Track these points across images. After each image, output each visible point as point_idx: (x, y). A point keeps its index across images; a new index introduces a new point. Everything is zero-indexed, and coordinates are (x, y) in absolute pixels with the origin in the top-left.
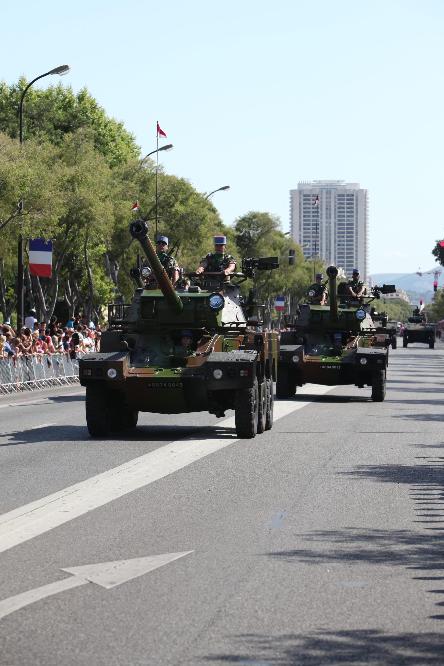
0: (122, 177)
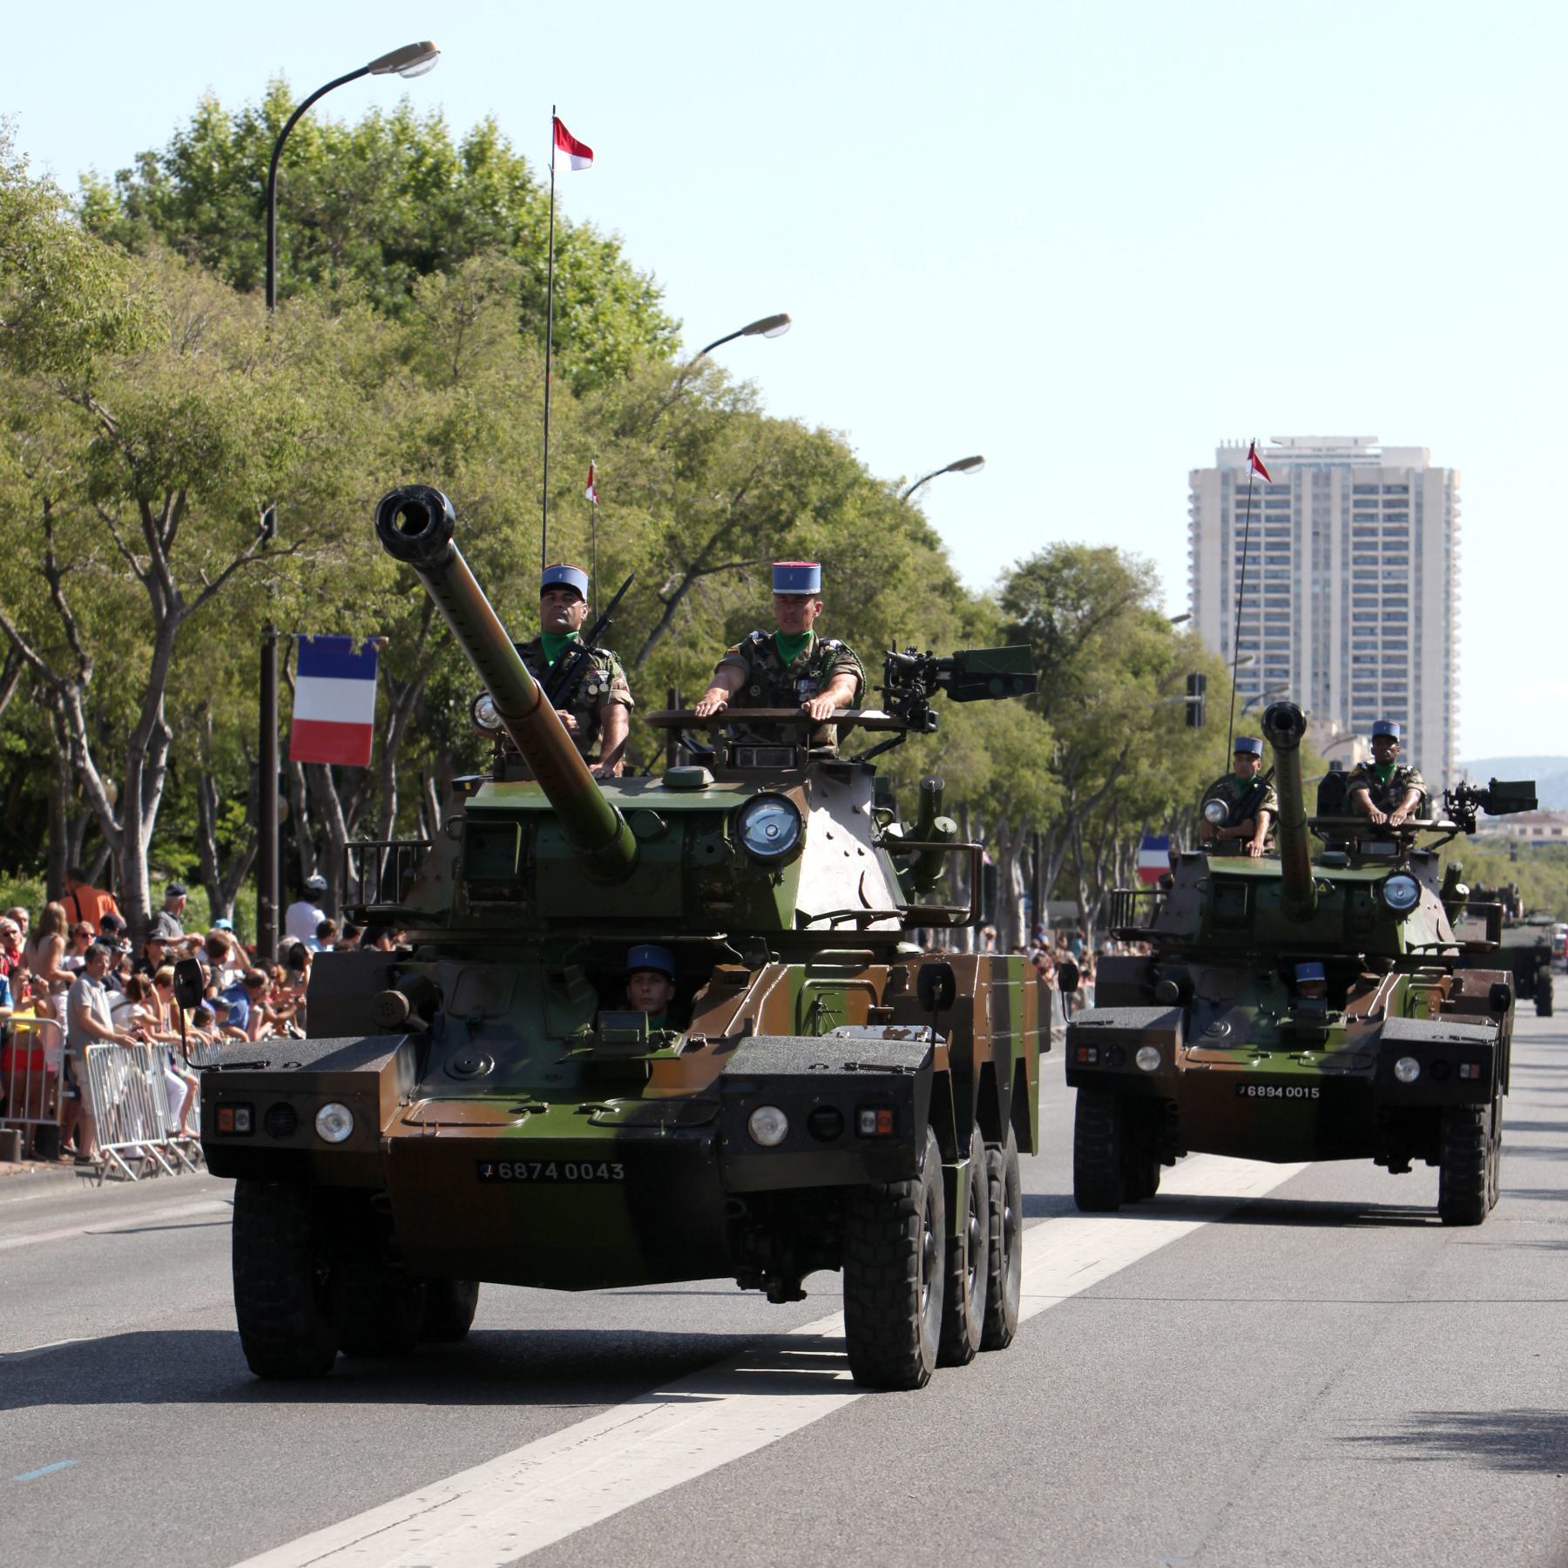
0: (615, 425)
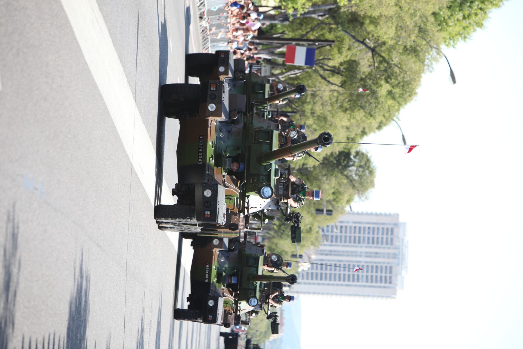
0: (422, 26)
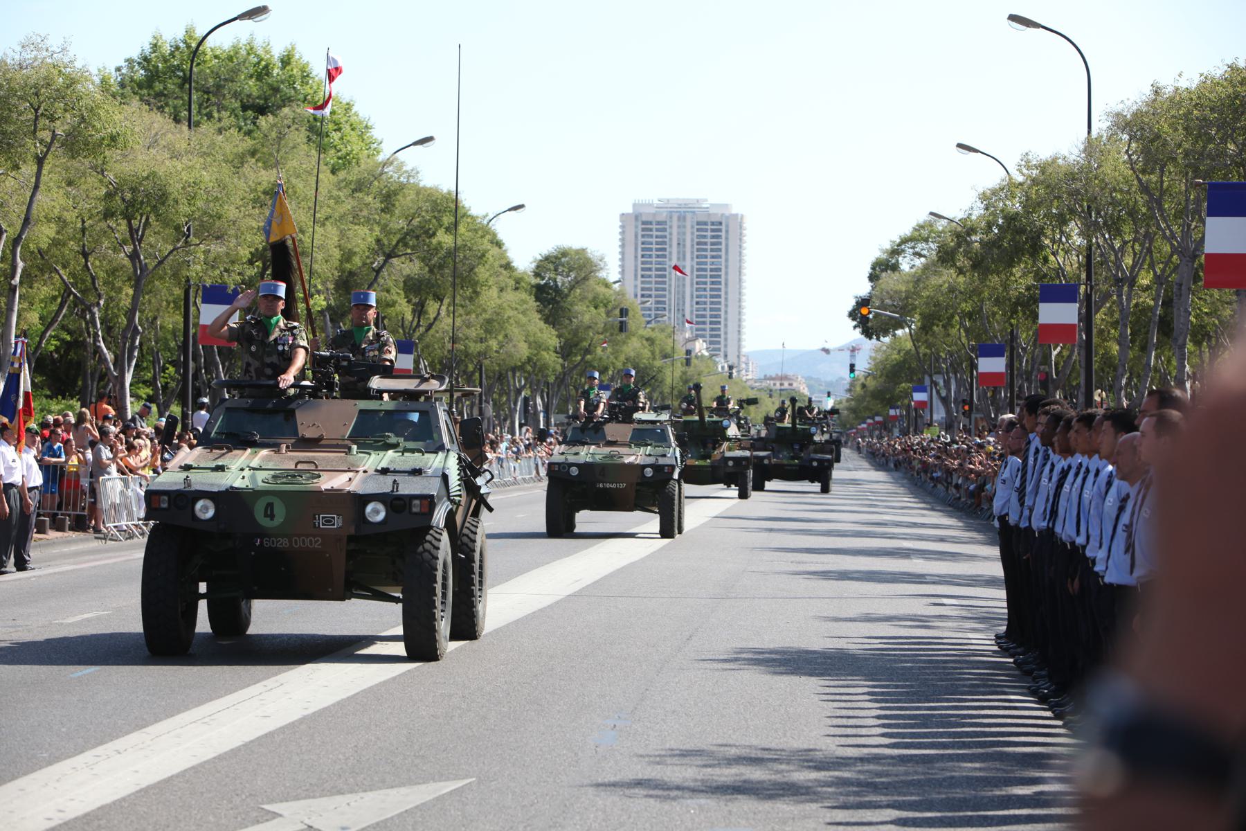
0: (353, 187)
